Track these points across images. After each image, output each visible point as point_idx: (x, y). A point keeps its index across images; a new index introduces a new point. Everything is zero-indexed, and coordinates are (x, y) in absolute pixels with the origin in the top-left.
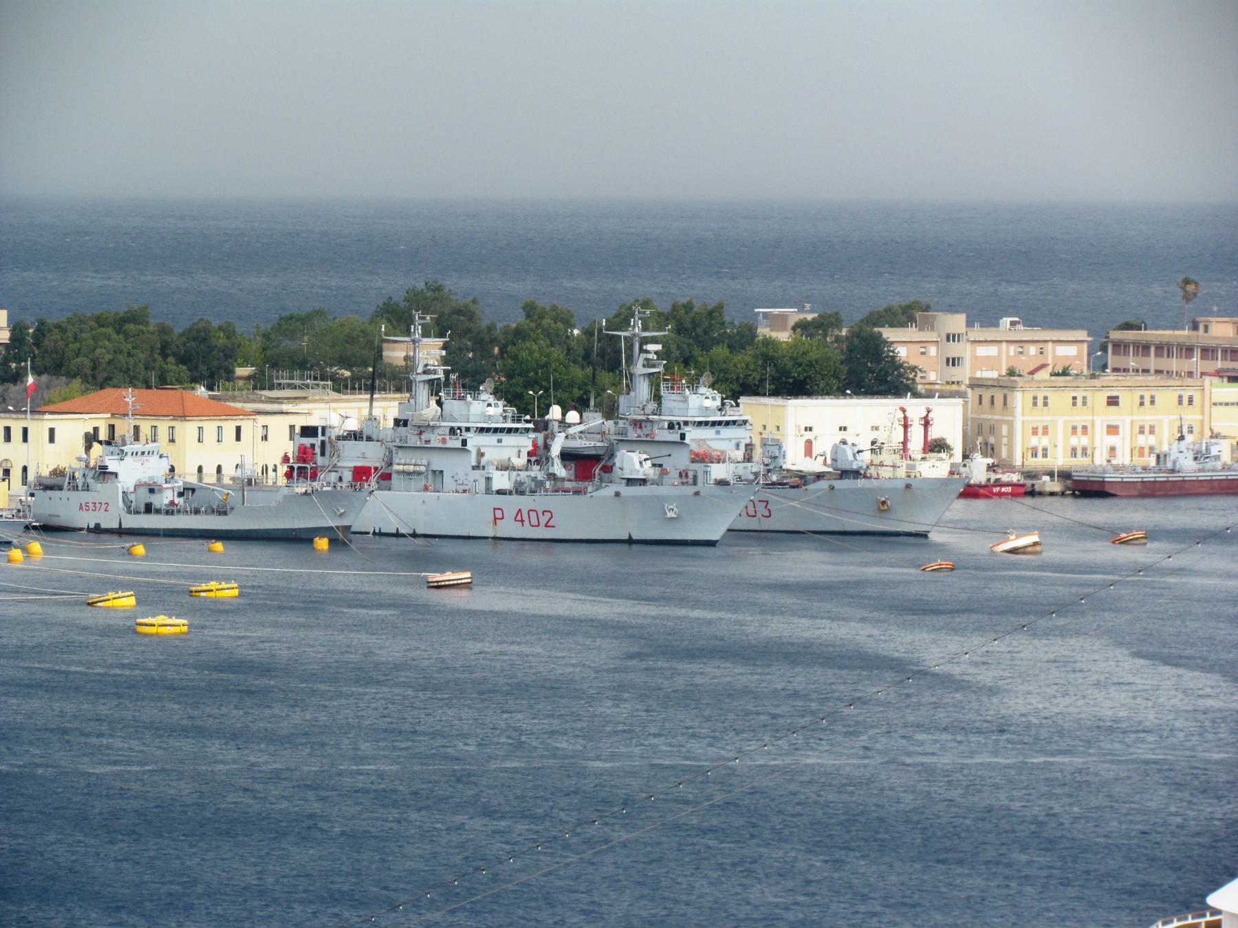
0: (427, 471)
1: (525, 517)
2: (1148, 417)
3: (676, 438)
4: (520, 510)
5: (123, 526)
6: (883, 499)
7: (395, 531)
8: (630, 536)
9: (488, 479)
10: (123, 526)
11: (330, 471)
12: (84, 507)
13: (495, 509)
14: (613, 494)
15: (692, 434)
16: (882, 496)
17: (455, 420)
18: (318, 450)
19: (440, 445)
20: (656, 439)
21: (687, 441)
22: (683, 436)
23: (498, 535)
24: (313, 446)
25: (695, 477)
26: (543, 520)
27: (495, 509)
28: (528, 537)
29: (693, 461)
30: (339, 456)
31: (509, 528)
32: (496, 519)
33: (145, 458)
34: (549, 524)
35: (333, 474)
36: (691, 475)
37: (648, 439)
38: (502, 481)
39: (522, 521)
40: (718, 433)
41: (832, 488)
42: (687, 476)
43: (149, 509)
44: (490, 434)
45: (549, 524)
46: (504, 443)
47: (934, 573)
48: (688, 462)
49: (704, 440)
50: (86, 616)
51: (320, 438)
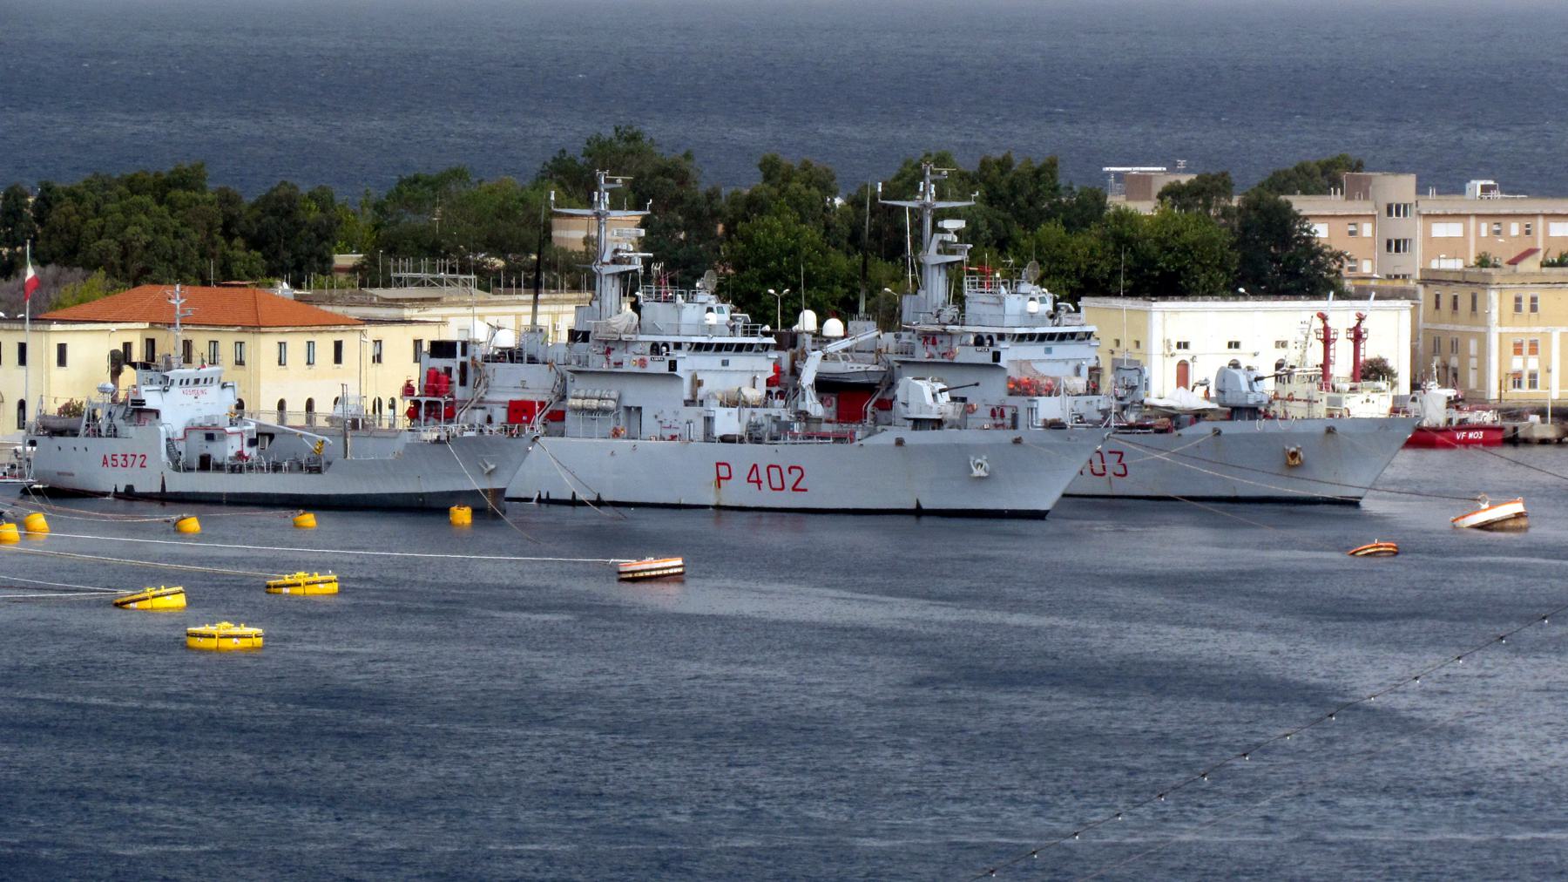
0: (617, 408)
1: (763, 477)
2: (1524, 330)
3: (986, 358)
4: (755, 466)
5: (168, 490)
6: (1293, 449)
7: (570, 498)
8: (918, 504)
9: (709, 420)
10: (168, 490)
11: (474, 408)
12: (110, 462)
13: (718, 464)
14: (893, 442)
15: (1011, 353)
16: (1291, 445)
17: (659, 333)
18: (456, 377)
19: (637, 369)
20: (957, 360)
21: (1003, 363)
22: (997, 357)
23: (722, 503)
24: (448, 370)
25: (1015, 417)
26: (790, 480)
27: (718, 464)
28: (662, 501)
29: (1012, 393)
30: (487, 386)
31: (739, 492)
32: (719, 478)
33: (199, 388)
34: (799, 486)
35: (478, 411)
36: (1008, 413)
37: (946, 360)
38: (728, 422)
39: (759, 482)
40: (1048, 351)
41: (1218, 433)
42: (1002, 415)
43: (205, 463)
44: (711, 352)
45: (799, 486)
46: (732, 366)
47: (1368, 559)
48: (1004, 395)
49: (1028, 362)
50: (113, 623)
51: (460, 358)
